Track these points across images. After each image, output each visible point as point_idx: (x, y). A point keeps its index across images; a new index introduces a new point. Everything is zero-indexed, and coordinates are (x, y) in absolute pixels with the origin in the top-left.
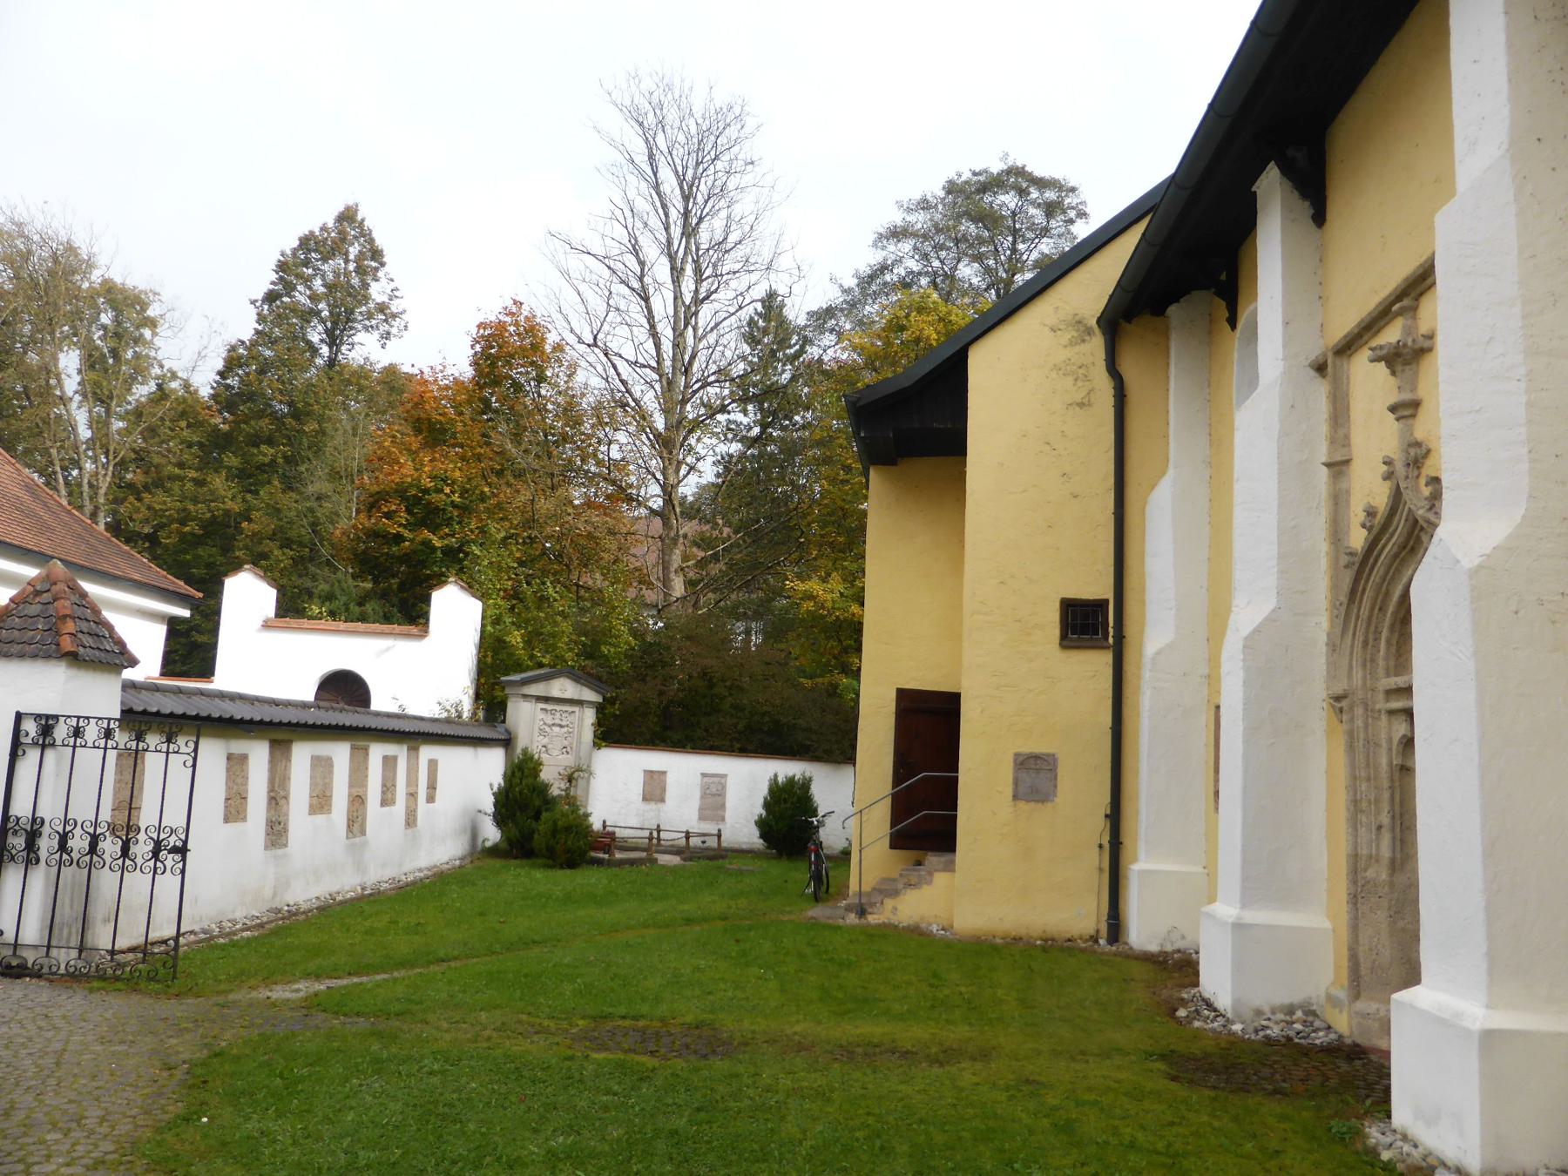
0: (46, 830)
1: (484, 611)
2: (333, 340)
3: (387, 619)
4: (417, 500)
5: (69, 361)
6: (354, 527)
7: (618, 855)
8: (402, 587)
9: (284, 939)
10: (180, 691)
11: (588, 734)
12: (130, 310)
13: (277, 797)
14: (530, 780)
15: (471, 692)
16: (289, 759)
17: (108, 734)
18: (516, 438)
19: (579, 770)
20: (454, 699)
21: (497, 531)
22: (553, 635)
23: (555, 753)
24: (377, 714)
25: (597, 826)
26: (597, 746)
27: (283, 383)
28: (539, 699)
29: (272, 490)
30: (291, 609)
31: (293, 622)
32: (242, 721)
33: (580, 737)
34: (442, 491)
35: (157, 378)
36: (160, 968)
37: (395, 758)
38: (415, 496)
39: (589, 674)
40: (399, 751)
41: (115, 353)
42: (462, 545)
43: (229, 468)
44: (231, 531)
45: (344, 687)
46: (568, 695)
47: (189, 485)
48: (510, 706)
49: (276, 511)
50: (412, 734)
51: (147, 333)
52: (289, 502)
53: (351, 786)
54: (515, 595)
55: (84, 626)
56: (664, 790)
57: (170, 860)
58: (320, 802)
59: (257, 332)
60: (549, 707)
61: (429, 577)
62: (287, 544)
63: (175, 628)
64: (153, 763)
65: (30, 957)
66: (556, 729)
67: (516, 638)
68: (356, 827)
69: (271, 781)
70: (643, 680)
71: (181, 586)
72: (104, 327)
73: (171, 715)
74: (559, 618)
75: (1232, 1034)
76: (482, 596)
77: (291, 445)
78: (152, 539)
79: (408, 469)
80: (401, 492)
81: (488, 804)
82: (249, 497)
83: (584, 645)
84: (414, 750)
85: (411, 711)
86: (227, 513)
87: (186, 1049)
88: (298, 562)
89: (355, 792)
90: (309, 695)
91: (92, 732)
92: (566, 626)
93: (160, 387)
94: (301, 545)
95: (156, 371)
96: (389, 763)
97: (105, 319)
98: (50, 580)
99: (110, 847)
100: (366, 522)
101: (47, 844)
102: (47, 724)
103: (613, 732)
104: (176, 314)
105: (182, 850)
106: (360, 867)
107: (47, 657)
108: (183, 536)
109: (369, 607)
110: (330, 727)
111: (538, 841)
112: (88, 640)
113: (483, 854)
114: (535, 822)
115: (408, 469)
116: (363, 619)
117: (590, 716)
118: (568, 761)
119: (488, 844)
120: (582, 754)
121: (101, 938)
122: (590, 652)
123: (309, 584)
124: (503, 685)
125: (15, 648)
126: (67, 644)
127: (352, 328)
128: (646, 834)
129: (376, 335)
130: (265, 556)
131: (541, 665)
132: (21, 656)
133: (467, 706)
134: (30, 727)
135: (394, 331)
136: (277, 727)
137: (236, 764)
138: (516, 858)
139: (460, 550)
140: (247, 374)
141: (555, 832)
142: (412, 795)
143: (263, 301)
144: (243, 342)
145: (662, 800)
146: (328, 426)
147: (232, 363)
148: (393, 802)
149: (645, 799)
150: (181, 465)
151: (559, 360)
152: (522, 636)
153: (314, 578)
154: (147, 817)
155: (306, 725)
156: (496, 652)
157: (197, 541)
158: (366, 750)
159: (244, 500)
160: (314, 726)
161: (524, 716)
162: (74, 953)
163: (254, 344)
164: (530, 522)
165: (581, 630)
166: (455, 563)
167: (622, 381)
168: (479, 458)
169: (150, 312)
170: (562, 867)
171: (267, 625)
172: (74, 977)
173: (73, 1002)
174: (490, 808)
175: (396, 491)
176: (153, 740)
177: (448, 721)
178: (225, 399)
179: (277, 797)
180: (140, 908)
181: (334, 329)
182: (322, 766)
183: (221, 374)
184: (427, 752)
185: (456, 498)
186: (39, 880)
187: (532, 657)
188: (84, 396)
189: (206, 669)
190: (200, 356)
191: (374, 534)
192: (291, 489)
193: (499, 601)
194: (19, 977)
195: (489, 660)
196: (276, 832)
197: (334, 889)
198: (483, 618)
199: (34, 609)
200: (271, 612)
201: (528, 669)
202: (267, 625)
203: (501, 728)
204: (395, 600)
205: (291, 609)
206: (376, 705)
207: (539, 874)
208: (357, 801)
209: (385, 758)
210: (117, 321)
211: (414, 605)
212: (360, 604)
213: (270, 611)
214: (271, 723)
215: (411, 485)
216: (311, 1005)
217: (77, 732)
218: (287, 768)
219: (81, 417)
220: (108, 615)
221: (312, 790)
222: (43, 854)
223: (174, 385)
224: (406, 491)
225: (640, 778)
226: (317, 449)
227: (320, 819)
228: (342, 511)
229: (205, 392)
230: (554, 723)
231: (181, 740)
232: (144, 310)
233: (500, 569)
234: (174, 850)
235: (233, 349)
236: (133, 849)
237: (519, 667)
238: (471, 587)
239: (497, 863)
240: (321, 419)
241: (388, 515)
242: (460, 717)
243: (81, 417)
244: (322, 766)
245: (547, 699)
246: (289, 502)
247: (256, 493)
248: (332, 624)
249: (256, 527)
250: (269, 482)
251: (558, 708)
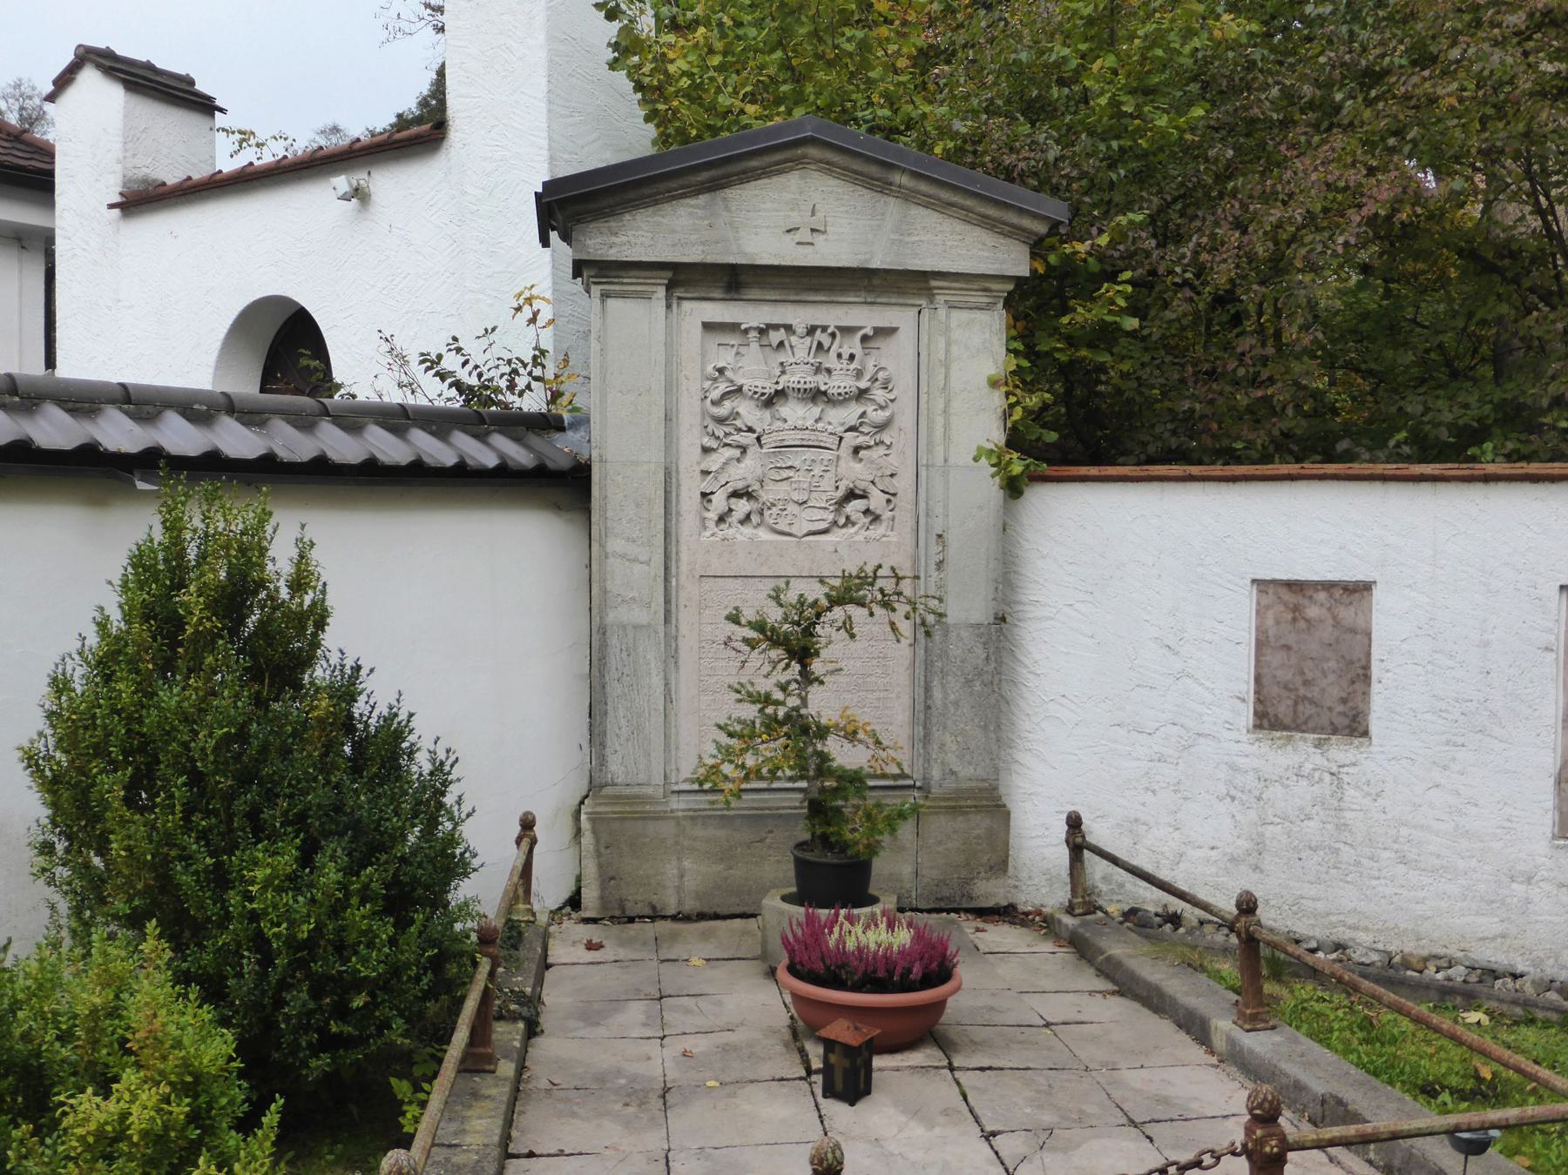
28: (683, 279)
46: (831, 252)
56: (1362, 676)
66: (794, 412)
75: (221, 587)
103: (1090, 414)
145: (1355, 727)
149: (1266, 720)
245: (734, 279)
251: (799, 316)
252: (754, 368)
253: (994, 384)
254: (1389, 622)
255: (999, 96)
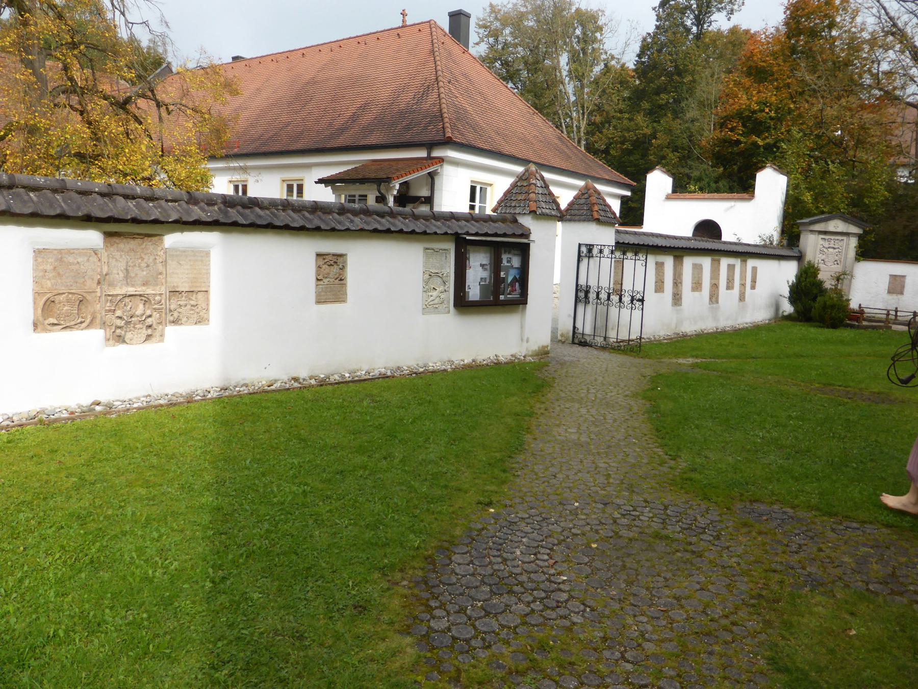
0: (591, 290)
1: (788, 182)
2: (699, 22)
3: (731, 190)
4: (749, 118)
5: (564, 59)
6: (713, 138)
7: (865, 323)
8: (740, 170)
9: (680, 344)
10: (627, 232)
11: (852, 253)
12: (589, 22)
13: (677, 282)
14: (812, 279)
15: (779, 230)
16: (682, 264)
17: (612, 252)
18: (813, 70)
19: (844, 274)
20: (768, 234)
21: (796, 133)
22: (831, 194)
23: (829, 264)
24: (725, 243)
25: (854, 305)
26: (857, 260)
27: (672, 55)
28: (820, 232)
29: (667, 120)
30: (680, 188)
31: (681, 196)
32: (661, 247)
33: (846, 255)
34: (764, 111)
35: (604, 60)
36: (634, 348)
37: (734, 266)
38: (747, 116)
39: (856, 217)
40: (737, 262)
41: (584, 50)
42: (776, 143)
43: (645, 110)
44: (646, 145)
45: (708, 229)
46: (839, 230)
47: (625, 122)
48: (802, 236)
49: (669, 131)
50: (743, 253)
51: (598, 35)
52: (677, 126)
53: (711, 279)
54: (806, 172)
55: (600, 207)
57: (638, 304)
58: (697, 286)
59: (657, 27)
60: (827, 237)
61: (756, 164)
62: (676, 149)
63: (624, 200)
64: (628, 264)
65: (588, 339)
66: (831, 250)
67: (808, 197)
68: (714, 299)
69: (675, 275)
70: (894, 219)
71: (627, 180)
72: (578, 37)
73: (634, 244)
74: (835, 184)
76: (787, 174)
77: (677, 92)
78: (606, 152)
79: (744, 99)
80: (739, 115)
81: (786, 292)
82: (655, 125)
83: (852, 199)
84: (744, 261)
85: (744, 241)
86: (644, 135)
87: (649, 372)
88: (682, 158)
89: (713, 282)
90: (689, 234)
91: (606, 251)
92: (840, 188)
93: (606, 65)
94: (683, 149)
95: (604, 56)
96: (731, 268)
97: (578, 32)
98: (587, 188)
99: (615, 298)
100: (718, 134)
101: (592, 296)
102: (590, 248)
104: (613, 23)
105: (642, 301)
106: (715, 318)
107: (589, 221)
108: (623, 150)
109: (720, 184)
110: (701, 249)
111: (814, 313)
112: (602, 213)
113: (781, 319)
114: (814, 302)
115: (744, 99)
116: (717, 191)
117: (853, 242)
118: (838, 268)
119: (785, 314)
120: (848, 264)
121: (612, 335)
122: (854, 203)
123: (687, 171)
124: (798, 225)
125: (577, 218)
126: (596, 215)
127: (709, 12)
128: (885, 312)
129: (725, 13)
130: (664, 158)
131: (823, 213)
132: (579, 221)
133: (776, 237)
134: (584, 249)
135: (736, 7)
136: (676, 250)
137: (660, 266)
138: (801, 321)
139: (775, 145)
140: (652, 54)
141: (825, 307)
142: (743, 285)
143: (660, 7)
144: (649, 34)
145: (902, 293)
146: (697, 77)
147: (645, 48)
148: (733, 288)
149: (889, 292)
150: (621, 112)
151: (844, 9)
152: (811, 195)
153: (690, 168)
154: (627, 286)
155: (690, 249)
156: (794, 206)
157: (629, 152)
158: (719, 261)
159: (654, 128)
160: (694, 249)
161: (812, 244)
162: (602, 339)
163: (655, 34)
164: (820, 124)
165: (849, 189)
166: (772, 155)
167: (891, 18)
168: (788, 86)
169: (600, 23)
170: (828, 327)
171: (668, 198)
172: (603, 348)
173: (605, 355)
174: (787, 294)
175: (737, 114)
176: (629, 255)
177: (764, 246)
178: (643, 70)
179: (677, 282)
180: (626, 324)
181: (699, 15)
182: (698, 268)
183: (639, 56)
184: (751, 263)
185: (773, 114)
186: (590, 309)
187: (817, 208)
188: (571, 78)
189: (639, 222)
190: (627, 44)
191: (725, 142)
192: (678, 118)
193: (798, 175)
194: (584, 346)
195: (790, 211)
196: (677, 299)
197: (703, 328)
198: (788, 186)
199: (582, 201)
200: (670, 191)
201: (815, 215)
202: (668, 198)
203: (796, 250)
204: (735, 178)
205: (680, 188)
206: (725, 238)
207: (813, 330)
208: (715, 286)
209: (729, 265)
210: (584, 34)
211: (746, 181)
212: (716, 182)
213: (669, 190)
214: (674, 248)
215: (745, 109)
216: (694, 366)
217: (601, 251)
218: (681, 269)
219: (570, 88)
220: (553, 189)
221: (693, 279)
222: (591, 300)
223: (613, 63)
224: (742, 113)
225: (887, 279)
226: (691, 91)
227: (697, 294)
228: (706, 127)
229: (631, 66)
230: (831, 248)
231: (640, 255)
232: (596, 22)
233: (799, 156)
234: (639, 300)
235: (644, 40)
236: (624, 299)
237: (809, 214)
238: (781, 169)
239: (790, 323)
240: (692, 73)
241: (732, 130)
242: (771, 244)
243: (570, 88)
244: (698, 268)
245: (825, 233)
246: (677, 126)
247: (659, 122)
248: (701, 195)
249: (659, 142)
250: (666, 115)
251: (832, 237)
252: (826, 244)
253: (203, 51)
254: (908, 281)
255: (745, 143)
